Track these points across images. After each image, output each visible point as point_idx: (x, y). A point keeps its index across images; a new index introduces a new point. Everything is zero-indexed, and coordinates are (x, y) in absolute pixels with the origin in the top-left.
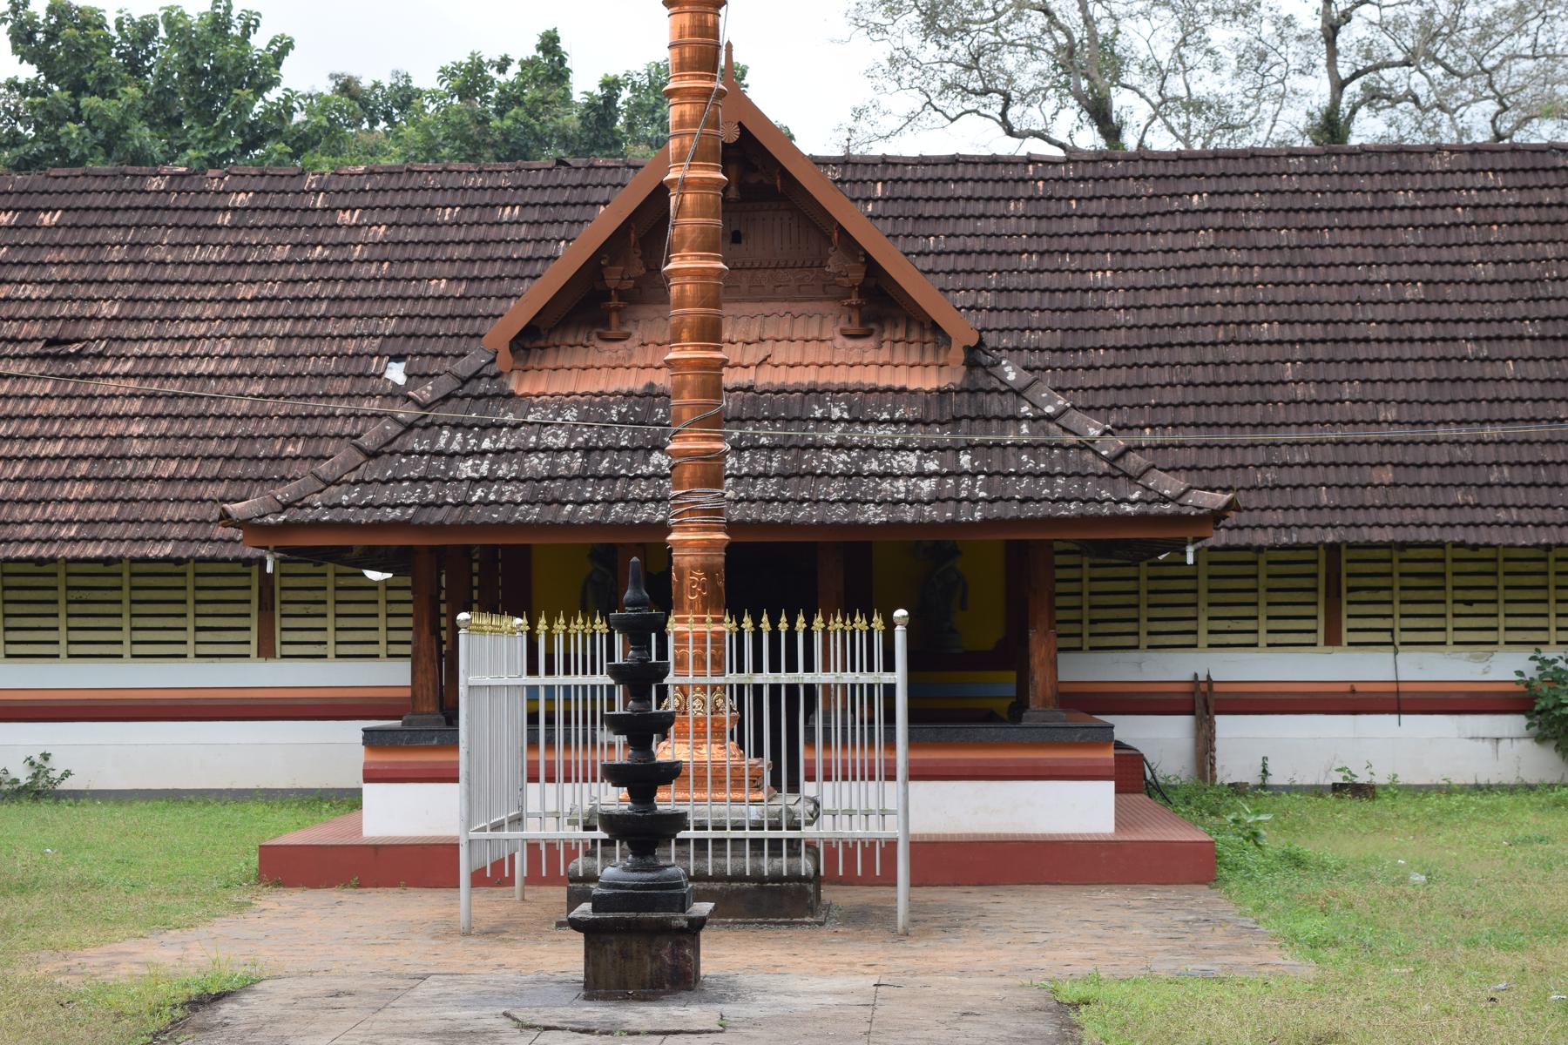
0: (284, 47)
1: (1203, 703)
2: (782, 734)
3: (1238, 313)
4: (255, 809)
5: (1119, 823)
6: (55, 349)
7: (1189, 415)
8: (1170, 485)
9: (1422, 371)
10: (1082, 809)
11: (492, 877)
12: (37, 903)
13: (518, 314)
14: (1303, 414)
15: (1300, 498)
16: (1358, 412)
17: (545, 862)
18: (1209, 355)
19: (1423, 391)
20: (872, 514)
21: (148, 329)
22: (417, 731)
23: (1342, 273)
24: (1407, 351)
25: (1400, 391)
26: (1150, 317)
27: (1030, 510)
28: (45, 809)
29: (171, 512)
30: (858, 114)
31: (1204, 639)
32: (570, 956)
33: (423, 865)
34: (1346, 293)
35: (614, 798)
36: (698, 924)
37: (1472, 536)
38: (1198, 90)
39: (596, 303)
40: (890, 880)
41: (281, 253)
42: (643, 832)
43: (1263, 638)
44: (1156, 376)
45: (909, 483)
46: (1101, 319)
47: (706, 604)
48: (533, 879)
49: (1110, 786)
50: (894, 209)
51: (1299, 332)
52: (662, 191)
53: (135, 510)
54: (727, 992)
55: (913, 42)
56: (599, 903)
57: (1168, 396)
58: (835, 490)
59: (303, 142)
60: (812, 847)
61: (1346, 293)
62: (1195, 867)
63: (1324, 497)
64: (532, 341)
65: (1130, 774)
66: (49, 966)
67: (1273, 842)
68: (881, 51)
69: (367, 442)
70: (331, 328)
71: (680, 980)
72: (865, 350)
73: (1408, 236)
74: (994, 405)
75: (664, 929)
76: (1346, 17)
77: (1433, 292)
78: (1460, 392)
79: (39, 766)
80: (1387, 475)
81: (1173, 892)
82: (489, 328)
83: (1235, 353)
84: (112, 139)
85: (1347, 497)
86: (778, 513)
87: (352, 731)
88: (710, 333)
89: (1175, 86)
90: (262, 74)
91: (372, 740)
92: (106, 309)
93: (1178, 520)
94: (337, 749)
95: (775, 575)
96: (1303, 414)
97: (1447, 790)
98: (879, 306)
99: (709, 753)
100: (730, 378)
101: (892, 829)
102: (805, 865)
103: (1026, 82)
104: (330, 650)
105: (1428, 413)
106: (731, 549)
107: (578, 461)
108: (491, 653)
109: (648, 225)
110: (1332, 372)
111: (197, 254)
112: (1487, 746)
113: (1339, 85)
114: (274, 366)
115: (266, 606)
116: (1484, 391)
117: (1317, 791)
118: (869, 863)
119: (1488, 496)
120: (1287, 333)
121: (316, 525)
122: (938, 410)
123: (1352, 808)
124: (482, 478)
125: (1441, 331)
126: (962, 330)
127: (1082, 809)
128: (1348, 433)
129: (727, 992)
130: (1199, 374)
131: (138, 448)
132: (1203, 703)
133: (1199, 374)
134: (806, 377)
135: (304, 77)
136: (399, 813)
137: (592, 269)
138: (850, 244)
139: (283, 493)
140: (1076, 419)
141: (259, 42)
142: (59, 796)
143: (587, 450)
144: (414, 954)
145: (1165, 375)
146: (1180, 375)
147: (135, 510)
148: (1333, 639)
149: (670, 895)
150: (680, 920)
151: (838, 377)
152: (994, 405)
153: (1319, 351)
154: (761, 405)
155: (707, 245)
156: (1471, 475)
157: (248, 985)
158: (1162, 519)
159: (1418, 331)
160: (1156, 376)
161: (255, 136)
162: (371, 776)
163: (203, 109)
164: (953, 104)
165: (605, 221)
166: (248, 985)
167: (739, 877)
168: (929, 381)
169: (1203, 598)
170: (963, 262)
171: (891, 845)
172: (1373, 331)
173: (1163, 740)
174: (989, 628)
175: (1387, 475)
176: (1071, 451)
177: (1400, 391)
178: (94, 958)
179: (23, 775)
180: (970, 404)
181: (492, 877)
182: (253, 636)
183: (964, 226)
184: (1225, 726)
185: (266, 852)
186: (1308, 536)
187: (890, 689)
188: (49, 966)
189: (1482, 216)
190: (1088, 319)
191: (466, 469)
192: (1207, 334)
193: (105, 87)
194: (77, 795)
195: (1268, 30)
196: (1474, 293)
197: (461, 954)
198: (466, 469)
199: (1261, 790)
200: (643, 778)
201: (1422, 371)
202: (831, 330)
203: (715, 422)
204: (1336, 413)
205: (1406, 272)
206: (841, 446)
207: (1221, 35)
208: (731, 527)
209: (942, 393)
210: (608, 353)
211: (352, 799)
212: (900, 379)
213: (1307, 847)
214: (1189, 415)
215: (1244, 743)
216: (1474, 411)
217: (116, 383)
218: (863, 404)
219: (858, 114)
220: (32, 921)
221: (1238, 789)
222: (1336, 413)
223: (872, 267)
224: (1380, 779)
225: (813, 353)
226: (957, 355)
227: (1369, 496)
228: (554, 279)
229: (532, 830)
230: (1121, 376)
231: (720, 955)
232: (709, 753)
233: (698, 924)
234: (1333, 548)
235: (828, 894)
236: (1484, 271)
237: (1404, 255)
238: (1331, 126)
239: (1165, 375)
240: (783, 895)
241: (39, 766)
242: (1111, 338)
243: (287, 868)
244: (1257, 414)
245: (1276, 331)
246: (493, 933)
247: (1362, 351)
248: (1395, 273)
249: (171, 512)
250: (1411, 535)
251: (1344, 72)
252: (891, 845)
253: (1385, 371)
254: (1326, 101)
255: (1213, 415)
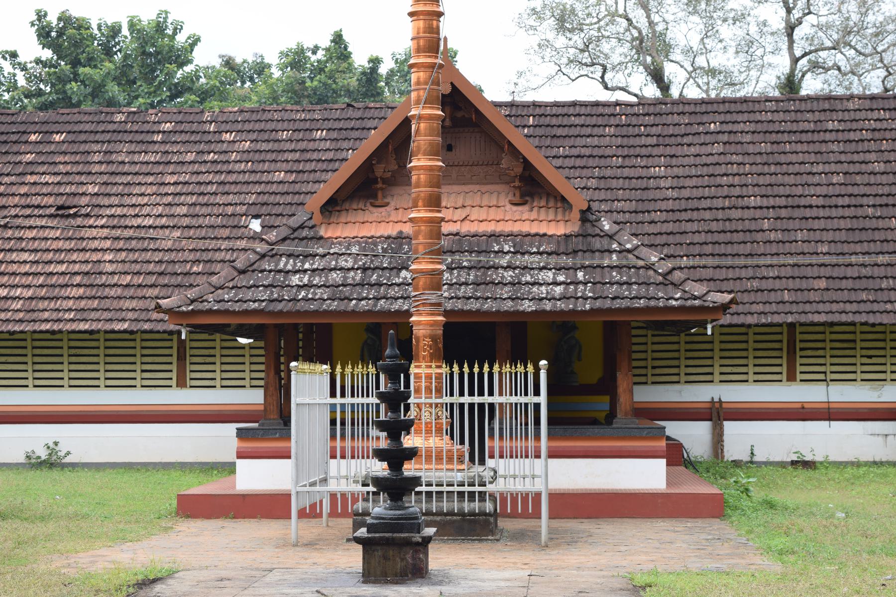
0: (195, 41)
1: (717, 414)
2: (475, 431)
3: (737, 191)
4: (175, 474)
5: (669, 483)
6: (62, 211)
7: (708, 249)
8: (698, 289)
9: (842, 224)
10: (648, 475)
11: (310, 513)
12: (51, 527)
13: (325, 192)
14: (774, 248)
15: (773, 297)
16: (806, 248)
17: (340, 505)
18: (720, 215)
19: (843, 235)
20: (527, 306)
21: (115, 200)
22: (268, 427)
23: (797, 168)
24: (834, 212)
25: (830, 236)
26: (686, 193)
27: (617, 304)
28: (55, 474)
29: (128, 304)
30: (520, 74)
31: (717, 377)
32: (354, 558)
33: (272, 506)
34: (799, 180)
35: (380, 468)
36: (427, 540)
37: (871, 319)
38: (714, 63)
39: (369, 185)
40: (537, 515)
41: (190, 157)
42: (396, 487)
43: (751, 377)
44: (689, 227)
45: (548, 289)
46: (658, 194)
47: (432, 357)
48: (333, 514)
49: (664, 461)
50: (540, 131)
51: (771, 202)
52: (407, 121)
53: (107, 303)
54: (444, 579)
55: (551, 35)
56: (371, 528)
57: (697, 238)
58: (506, 292)
59: (205, 95)
60: (492, 496)
61: (799, 180)
62: (712, 508)
63: (786, 296)
64: (332, 207)
65: (675, 455)
66: (58, 563)
67: (758, 494)
68: (535, 40)
69: (239, 265)
70: (219, 199)
71: (417, 572)
72: (523, 212)
73: (834, 147)
74: (597, 243)
75: (408, 543)
76: (800, 22)
77: (849, 179)
78: (864, 236)
79: (52, 449)
80: (823, 284)
81: (699, 522)
82: (308, 199)
83: (735, 214)
84: (97, 91)
85: (800, 296)
86: (473, 305)
87: (231, 429)
88: (434, 202)
89: (701, 61)
90: (181, 58)
91: (242, 434)
92: (91, 189)
93: (702, 309)
94: (221, 440)
95: (472, 341)
96: (774, 248)
97: (857, 464)
98: (531, 187)
99: (434, 442)
100: (446, 228)
101: (539, 486)
102: (489, 506)
103: (616, 59)
104: (218, 383)
105: (846, 248)
106: (446, 326)
107: (359, 276)
108: (309, 384)
109: (399, 141)
110: (791, 225)
111: (143, 158)
112: (880, 439)
113: (795, 61)
114: (186, 221)
115: (181, 358)
116: (878, 236)
117: (782, 465)
118: (525, 506)
119: (881, 296)
120: (765, 202)
121: (210, 312)
122: (565, 246)
123: (803, 474)
124: (306, 285)
125: (853, 201)
126: (579, 201)
127: (648, 475)
128: (800, 260)
129: (444, 579)
130: (714, 226)
131: (109, 268)
132: (717, 414)
133: (714, 226)
134: (489, 228)
135: (205, 57)
136: (257, 476)
137: (367, 166)
138: (514, 151)
139: (191, 294)
140: (644, 251)
141: (181, 39)
142: (63, 466)
143: (365, 269)
144: (266, 557)
145: (695, 226)
146: (703, 226)
147: (107, 303)
148: (791, 378)
149: (411, 524)
150: (417, 538)
151: (508, 228)
152: (597, 243)
153: (784, 213)
154: (463, 243)
155: (433, 152)
156: (871, 284)
157: (171, 574)
158: (693, 309)
159: (840, 201)
160: (689, 227)
161: (178, 91)
162: (241, 455)
163: (149, 75)
164: (574, 71)
165: (375, 139)
166: (171, 574)
167: (451, 513)
168: (559, 230)
169: (717, 354)
170: (579, 162)
171: (538, 495)
172: (814, 201)
173: (693, 436)
174: (595, 370)
175: (823, 284)
176: (638, 271)
177: (830, 236)
178: (83, 558)
179: (43, 454)
180: (584, 242)
181: (310, 513)
182: (174, 375)
183: (580, 141)
184: (730, 427)
185: (181, 498)
186: (777, 319)
187: (537, 406)
188: (58, 563)
189: (877, 135)
190: (651, 195)
191: (295, 280)
192: (719, 203)
193: (91, 61)
194: (73, 466)
195: (753, 29)
196: (872, 179)
197: (292, 557)
198: (295, 280)
199: (751, 464)
200: (396, 457)
201: (842, 224)
202: (504, 201)
203: (438, 252)
204: (793, 248)
205: (833, 167)
206: (509, 267)
207: (726, 31)
208: (446, 313)
209: (567, 236)
210: (376, 213)
211: (229, 468)
212: (543, 229)
213: (776, 496)
214: (708, 249)
215: (740, 437)
216: (872, 247)
217: (96, 232)
218: (522, 243)
219: (520, 74)
220: (48, 538)
221: (737, 464)
222: (793, 248)
223: (527, 165)
224: (819, 458)
225: (493, 214)
226: (576, 215)
227: (813, 296)
228: (345, 172)
229: (333, 486)
230: (670, 227)
231: (440, 557)
232: (434, 442)
233: (427, 540)
234: (792, 326)
235: (502, 523)
236: (878, 167)
237: (832, 157)
238: (791, 84)
239: (695, 226)
240: (475, 524)
241: (401, 232)
242: (664, 205)
243: (193, 507)
244: (748, 249)
245: (759, 201)
246: (310, 545)
247: (808, 213)
248: (827, 168)
249: (128, 304)
250: (836, 318)
251: (798, 53)
252: (538, 495)
253: (821, 224)
254: (787, 70)
255: (722, 249)
